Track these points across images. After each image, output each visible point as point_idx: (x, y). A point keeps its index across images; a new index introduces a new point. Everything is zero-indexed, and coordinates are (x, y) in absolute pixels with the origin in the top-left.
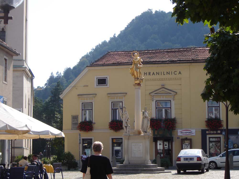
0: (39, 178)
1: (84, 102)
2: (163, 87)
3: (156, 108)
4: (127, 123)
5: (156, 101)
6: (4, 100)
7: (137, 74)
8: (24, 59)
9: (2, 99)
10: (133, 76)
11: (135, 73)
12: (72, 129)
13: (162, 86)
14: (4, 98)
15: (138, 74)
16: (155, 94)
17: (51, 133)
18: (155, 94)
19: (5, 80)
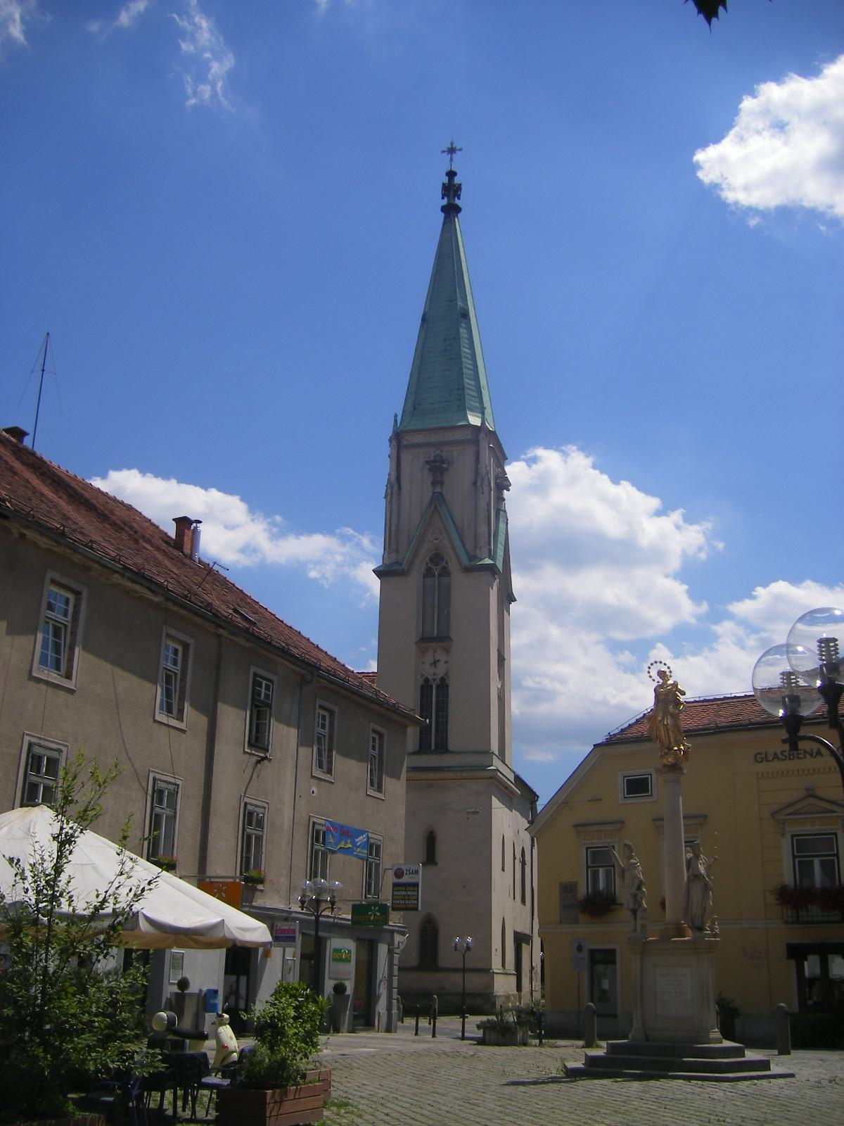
0: (103, 1097)
1: (592, 843)
2: (811, 793)
3: (794, 857)
4: (638, 898)
5: (793, 836)
6: (372, 841)
7: (668, 733)
8: (494, 747)
9: (361, 837)
10: (658, 742)
11: (663, 732)
12: (561, 923)
13: (807, 790)
14: (370, 835)
15: (671, 733)
16: (835, 812)
17: (148, 919)
18: (835, 812)
19: (378, 787)
